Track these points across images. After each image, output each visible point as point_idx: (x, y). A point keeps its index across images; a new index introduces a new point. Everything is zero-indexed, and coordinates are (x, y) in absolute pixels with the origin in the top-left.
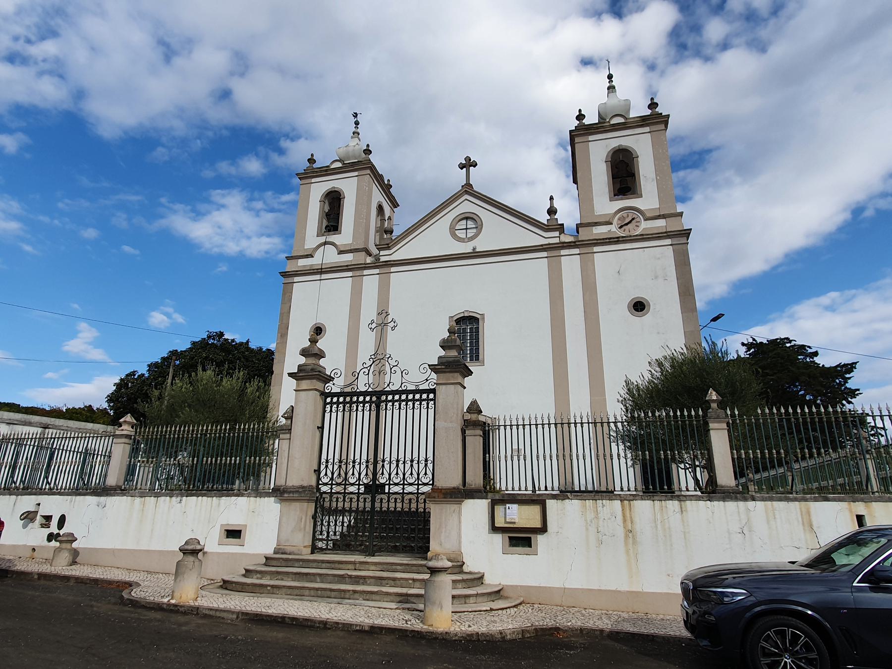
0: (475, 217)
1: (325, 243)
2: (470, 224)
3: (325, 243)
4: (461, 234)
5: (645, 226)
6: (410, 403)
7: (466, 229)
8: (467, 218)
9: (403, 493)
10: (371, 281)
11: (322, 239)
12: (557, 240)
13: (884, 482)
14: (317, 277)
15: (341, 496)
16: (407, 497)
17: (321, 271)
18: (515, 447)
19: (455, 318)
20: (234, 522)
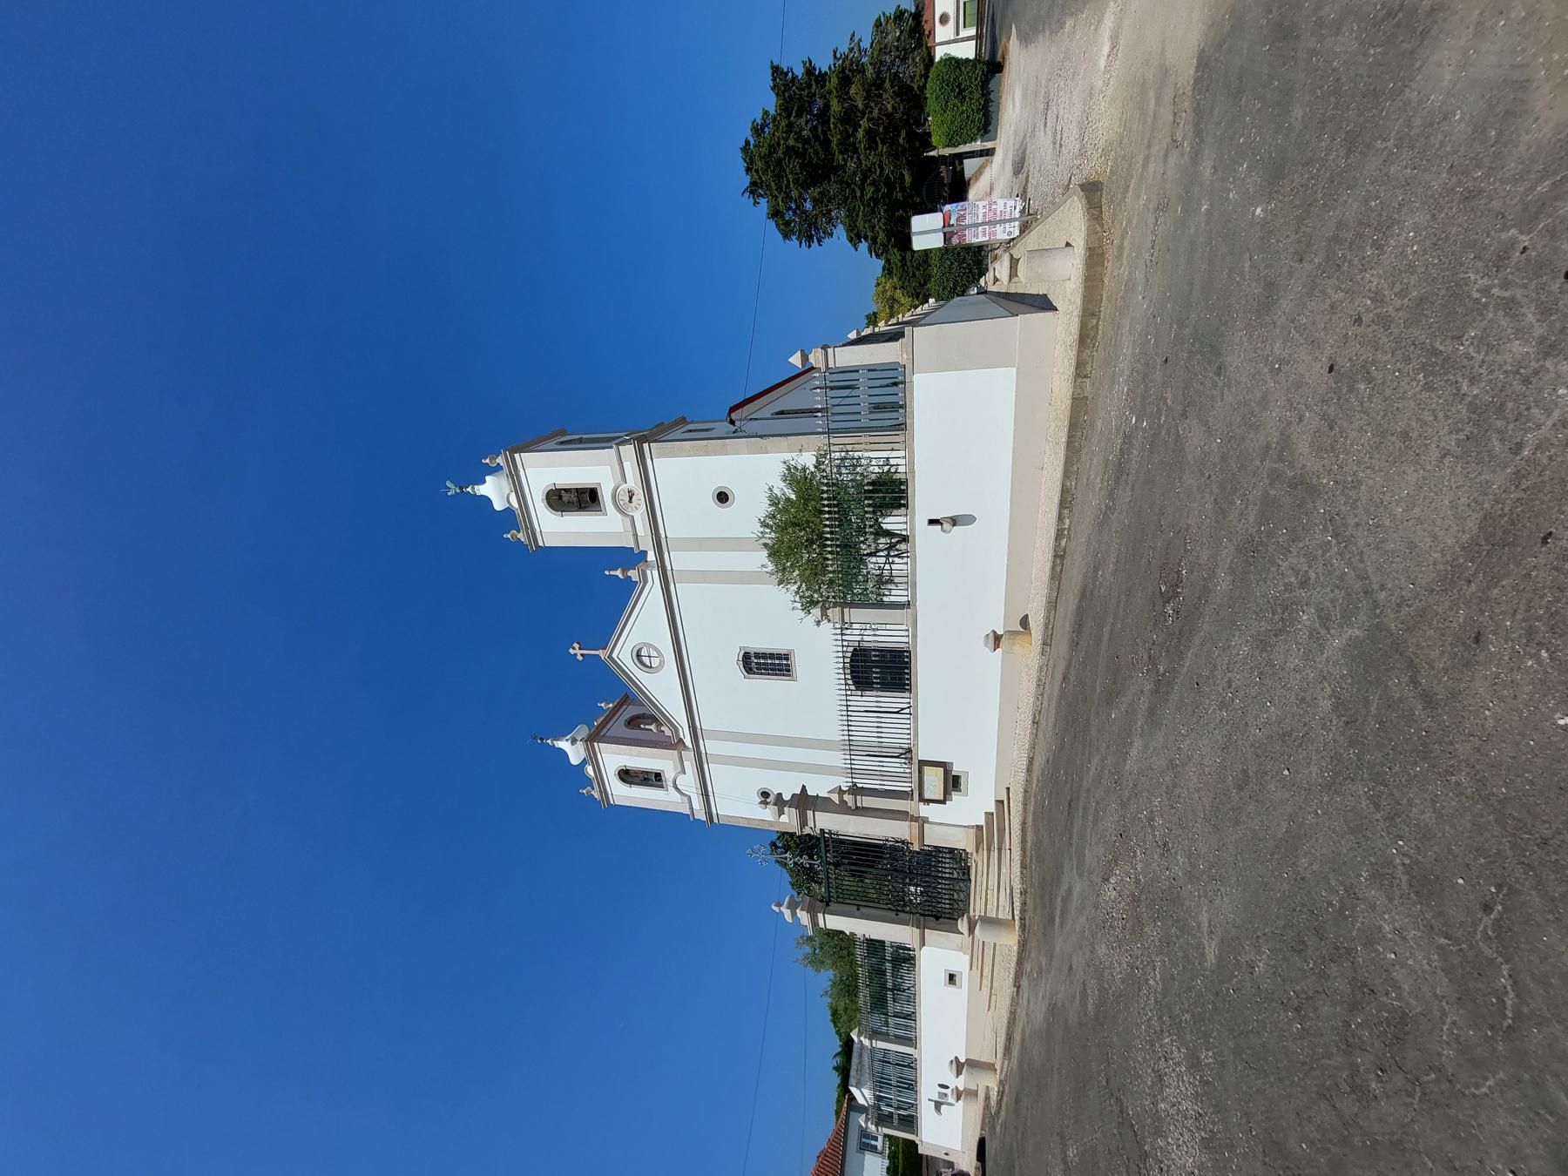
8: (639, 656)
12: (655, 573)
20: (944, 978)
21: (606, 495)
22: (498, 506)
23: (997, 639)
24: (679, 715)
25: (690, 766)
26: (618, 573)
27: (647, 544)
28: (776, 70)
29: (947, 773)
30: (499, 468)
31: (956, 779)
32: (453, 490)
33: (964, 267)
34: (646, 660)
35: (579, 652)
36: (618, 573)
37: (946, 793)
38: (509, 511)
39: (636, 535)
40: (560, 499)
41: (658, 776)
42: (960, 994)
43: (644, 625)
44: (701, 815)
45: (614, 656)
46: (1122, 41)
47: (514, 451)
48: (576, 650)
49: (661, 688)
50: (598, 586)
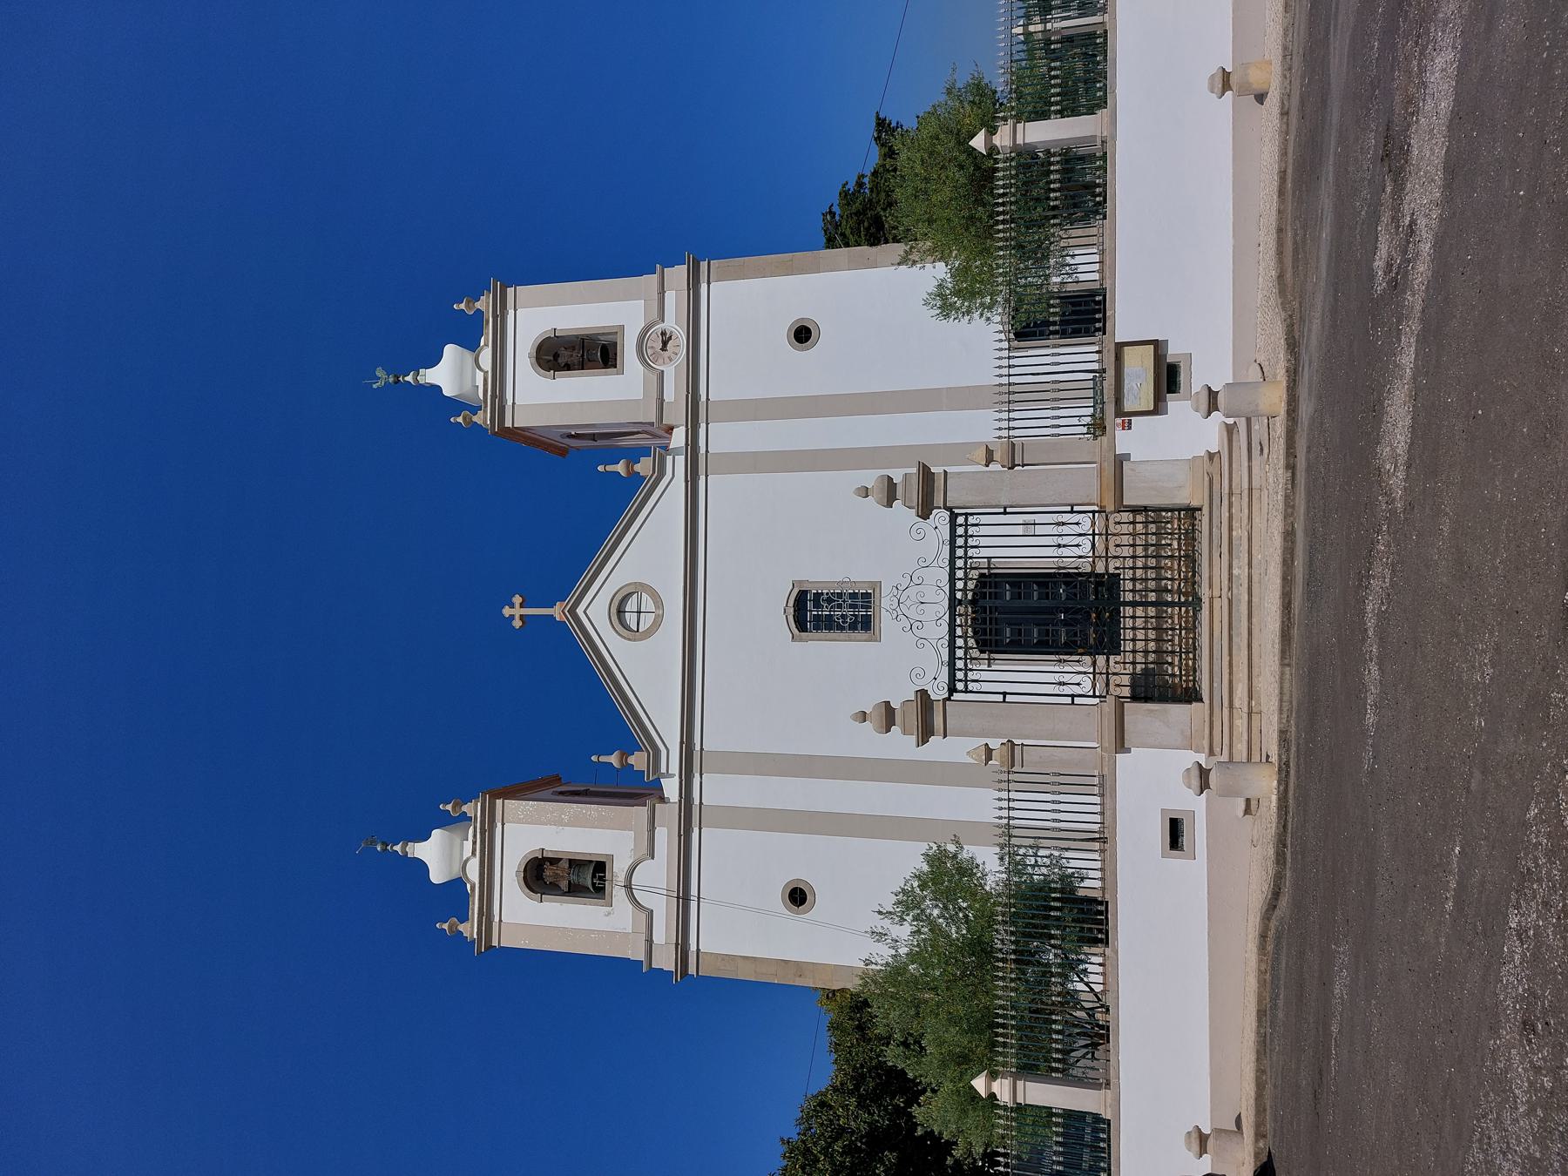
0: (614, 610)
1: (628, 887)
2: (631, 605)
3: (628, 887)
4: (647, 621)
5: (674, 322)
6: (971, 552)
7: (639, 612)
8: (621, 612)
9: (1107, 557)
10: (714, 789)
11: (619, 894)
12: (680, 460)
13: (1086, 8)
14: (693, 905)
15: (1112, 540)
16: (1113, 551)
17: (683, 898)
18: (1020, 530)
19: (796, 631)
20: (1158, 834)
21: (619, 869)
22: (437, 877)
23: (1203, 1140)
24: (665, 724)
25: (665, 837)
26: (613, 759)
27: (676, 414)
28: (882, 124)
32: (382, 377)
33: (965, 1112)
34: (631, 619)
35: (518, 611)
36: (613, 759)
38: (457, 886)
39: (661, 401)
40: (542, 875)
41: (600, 867)
42: (1193, 869)
43: (647, 551)
44: (665, 960)
45: (580, 611)
47: (496, 795)
48: (515, 611)
49: (645, 673)
50: (581, 490)
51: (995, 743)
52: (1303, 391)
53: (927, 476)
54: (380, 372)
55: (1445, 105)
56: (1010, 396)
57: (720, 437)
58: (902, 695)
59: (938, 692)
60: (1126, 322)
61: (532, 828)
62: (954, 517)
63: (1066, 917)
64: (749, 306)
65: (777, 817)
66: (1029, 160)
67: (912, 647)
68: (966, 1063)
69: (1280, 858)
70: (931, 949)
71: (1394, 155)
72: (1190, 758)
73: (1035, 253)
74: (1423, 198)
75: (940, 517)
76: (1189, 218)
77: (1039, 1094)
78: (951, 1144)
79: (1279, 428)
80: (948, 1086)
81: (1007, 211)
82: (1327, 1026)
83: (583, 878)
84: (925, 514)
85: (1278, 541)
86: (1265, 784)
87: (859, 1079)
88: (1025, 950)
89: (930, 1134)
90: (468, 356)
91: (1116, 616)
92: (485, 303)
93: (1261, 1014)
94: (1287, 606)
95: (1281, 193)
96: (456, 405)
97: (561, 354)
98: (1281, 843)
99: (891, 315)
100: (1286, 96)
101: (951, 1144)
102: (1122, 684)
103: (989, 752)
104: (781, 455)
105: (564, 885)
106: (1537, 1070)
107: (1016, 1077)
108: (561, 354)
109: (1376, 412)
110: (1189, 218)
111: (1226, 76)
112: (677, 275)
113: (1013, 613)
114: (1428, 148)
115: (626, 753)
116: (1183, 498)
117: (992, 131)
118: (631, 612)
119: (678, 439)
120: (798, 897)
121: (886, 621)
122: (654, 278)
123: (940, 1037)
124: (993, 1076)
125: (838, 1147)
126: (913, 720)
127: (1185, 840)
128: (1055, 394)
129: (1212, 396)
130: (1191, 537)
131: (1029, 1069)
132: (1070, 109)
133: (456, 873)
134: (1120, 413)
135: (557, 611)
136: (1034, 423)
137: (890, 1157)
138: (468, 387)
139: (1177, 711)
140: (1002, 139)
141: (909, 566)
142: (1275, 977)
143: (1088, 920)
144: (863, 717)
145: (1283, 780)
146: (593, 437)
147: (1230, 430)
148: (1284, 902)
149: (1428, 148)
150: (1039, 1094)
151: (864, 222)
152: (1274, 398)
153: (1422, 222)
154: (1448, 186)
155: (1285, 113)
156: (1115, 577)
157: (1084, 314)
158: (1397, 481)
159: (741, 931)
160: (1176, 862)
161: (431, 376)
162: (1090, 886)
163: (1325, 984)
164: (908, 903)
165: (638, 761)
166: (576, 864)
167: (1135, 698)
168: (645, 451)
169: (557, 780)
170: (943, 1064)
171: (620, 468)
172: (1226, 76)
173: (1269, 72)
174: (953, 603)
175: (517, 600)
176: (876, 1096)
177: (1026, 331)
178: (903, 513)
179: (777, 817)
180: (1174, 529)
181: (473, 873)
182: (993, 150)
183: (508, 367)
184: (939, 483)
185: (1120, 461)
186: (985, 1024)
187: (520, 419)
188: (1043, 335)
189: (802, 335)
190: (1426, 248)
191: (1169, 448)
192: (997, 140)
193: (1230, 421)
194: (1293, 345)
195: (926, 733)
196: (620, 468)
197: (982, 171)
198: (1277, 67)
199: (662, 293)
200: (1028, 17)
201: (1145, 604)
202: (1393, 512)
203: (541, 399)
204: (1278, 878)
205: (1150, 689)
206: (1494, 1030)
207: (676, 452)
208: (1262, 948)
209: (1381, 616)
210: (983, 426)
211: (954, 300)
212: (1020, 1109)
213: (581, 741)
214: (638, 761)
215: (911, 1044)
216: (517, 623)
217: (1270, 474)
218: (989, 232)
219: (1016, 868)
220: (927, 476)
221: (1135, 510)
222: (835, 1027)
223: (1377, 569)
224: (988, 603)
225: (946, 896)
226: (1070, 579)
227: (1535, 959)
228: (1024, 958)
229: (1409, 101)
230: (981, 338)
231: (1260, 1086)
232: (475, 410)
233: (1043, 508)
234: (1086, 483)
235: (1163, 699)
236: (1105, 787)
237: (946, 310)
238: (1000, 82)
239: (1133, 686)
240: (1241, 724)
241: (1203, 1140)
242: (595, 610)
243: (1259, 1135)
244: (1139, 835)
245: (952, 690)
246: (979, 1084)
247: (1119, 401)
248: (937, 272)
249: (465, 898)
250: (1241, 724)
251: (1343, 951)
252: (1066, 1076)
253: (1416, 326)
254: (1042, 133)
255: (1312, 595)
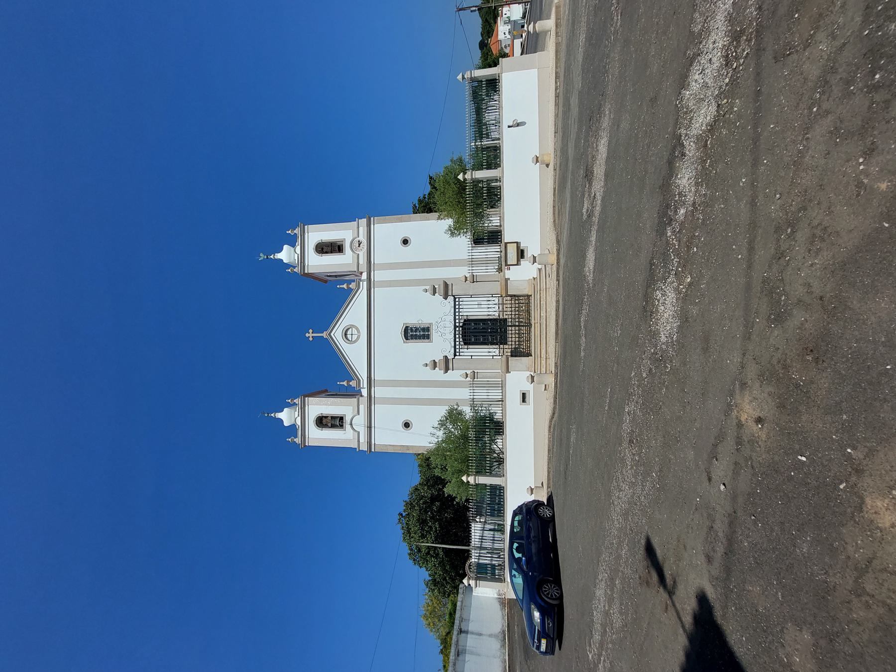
2: (349, 332)
3: (351, 424)
4: (355, 337)
5: (363, 238)
8: (346, 334)
11: (348, 427)
12: (365, 283)
17: (370, 427)
20: (519, 398)
21: (347, 419)
22: (286, 424)
23: (532, 490)
24: (363, 374)
25: (363, 408)
26: (345, 383)
28: (431, 178)
29: (518, 247)
30: (295, 404)
31: (522, 251)
32: (262, 256)
34: (349, 337)
35: (311, 335)
36: (345, 383)
37: (518, 261)
38: (293, 427)
40: (321, 422)
42: (529, 408)
43: (354, 314)
44: (364, 447)
46: (561, 279)
47: (305, 396)
48: (310, 335)
49: (354, 355)
50: (332, 293)
51: (469, 372)
52: (561, 256)
53: (446, 285)
54: (261, 255)
55: (604, 156)
56: (472, 262)
57: (378, 276)
58: (439, 358)
59: (451, 356)
60: (507, 237)
61: (318, 407)
62: (455, 299)
63: (490, 426)
64: (387, 232)
65: (397, 395)
66: (476, 182)
67: (443, 341)
68: (461, 472)
69: (555, 402)
70: (446, 437)
71: (589, 175)
72: (528, 374)
73: (480, 216)
74: (598, 186)
75: (451, 299)
76: (526, 205)
77: (483, 480)
78: (455, 497)
79: (555, 268)
80: (454, 480)
81: (469, 200)
82: (569, 452)
83: (337, 422)
84: (446, 298)
85: (554, 304)
86: (550, 380)
87: (428, 481)
88: (477, 437)
89: (449, 496)
90: (292, 249)
91: (506, 331)
92: (297, 231)
93: (549, 450)
94: (557, 324)
95: (554, 195)
96: (288, 266)
97: (324, 248)
98: (555, 398)
99: (436, 239)
100: (555, 165)
101: (455, 497)
102: (508, 352)
103: (467, 375)
104: (398, 277)
105: (330, 425)
106: (634, 455)
107: (475, 475)
108: (324, 248)
109: (584, 257)
110: (526, 205)
111: (537, 158)
112: (363, 222)
113: (475, 332)
114: (599, 170)
115: (349, 381)
116: (526, 292)
117: (465, 173)
118: (348, 335)
119: (364, 276)
120: (407, 425)
121: (434, 334)
122: (356, 223)
123: (452, 465)
124: (468, 475)
125: (421, 502)
126: (443, 365)
127: (527, 399)
128: (486, 262)
129: (534, 258)
130: (528, 305)
131: (479, 473)
132: (489, 167)
133: (293, 422)
134: (506, 265)
135: (324, 335)
136: (479, 271)
137: (438, 504)
138: (292, 260)
139: (524, 360)
140: (468, 176)
141: (440, 316)
142: (553, 439)
143: (498, 428)
144: (426, 365)
145: (556, 378)
146: (336, 276)
147: (540, 270)
148: (556, 415)
149: (599, 170)
150: (483, 480)
151: (426, 207)
152: (553, 259)
153: (598, 194)
154: (606, 180)
155: (555, 170)
156: (506, 319)
157: (494, 237)
158: (590, 278)
159: (389, 436)
160: (524, 406)
161: (279, 256)
162: (498, 417)
163: (568, 438)
164: (442, 424)
165: (353, 383)
166: (333, 418)
167: (512, 356)
168: (354, 281)
169: (326, 391)
170: (453, 474)
171: (345, 286)
172: (537, 158)
173: (551, 158)
174: (455, 327)
175: (311, 331)
176: (433, 486)
177: (478, 241)
178: (438, 297)
179: (397, 395)
180: (522, 303)
181: (299, 422)
182: (465, 179)
183: (304, 252)
184: (450, 287)
185: (507, 280)
186: (466, 460)
187: (310, 270)
188: (482, 243)
189: (405, 242)
190: (599, 202)
191: (521, 276)
192: (466, 176)
193: (540, 267)
194: (558, 242)
195: (447, 369)
196: (345, 286)
197: (462, 185)
198: (552, 155)
199: (358, 227)
200: (476, 140)
201: (515, 326)
202: (589, 288)
203: (317, 263)
204: (554, 408)
205: (516, 353)
206: (620, 445)
207: (363, 281)
208: (549, 430)
209: (585, 321)
210: (465, 271)
211: (454, 231)
212: (477, 485)
213: (334, 377)
214: (353, 383)
215: (444, 469)
216: (311, 339)
217: (552, 283)
218: (464, 207)
219: (476, 412)
220: (446, 285)
221: (511, 296)
222: (420, 466)
223: (584, 307)
224: (466, 327)
225: (454, 422)
226: (494, 321)
227: (633, 420)
228: (478, 439)
229: (593, 157)
230: (464, 241)
231: (549, 472)
232: (294, 267)
233: (483, 295)
234: (497, 288)
235: (520, 356)
236: (503, 386)
237: (452, 234)
238: (467, 158)
239: (511, 352)
240: (543, 362)
241: (532, 490)
242: (337, 334)
243: (548, 487)
244: (512, 398)
245: (455, 355)
246: (464, 478)
247: (506, 261)
248: (450, 222)
249: (297, 430)
250: (543, 362)
251: (574, 428)
252: (491, 474)
253: (596, 227)
254: (480, 174)
255: (564, 320)
